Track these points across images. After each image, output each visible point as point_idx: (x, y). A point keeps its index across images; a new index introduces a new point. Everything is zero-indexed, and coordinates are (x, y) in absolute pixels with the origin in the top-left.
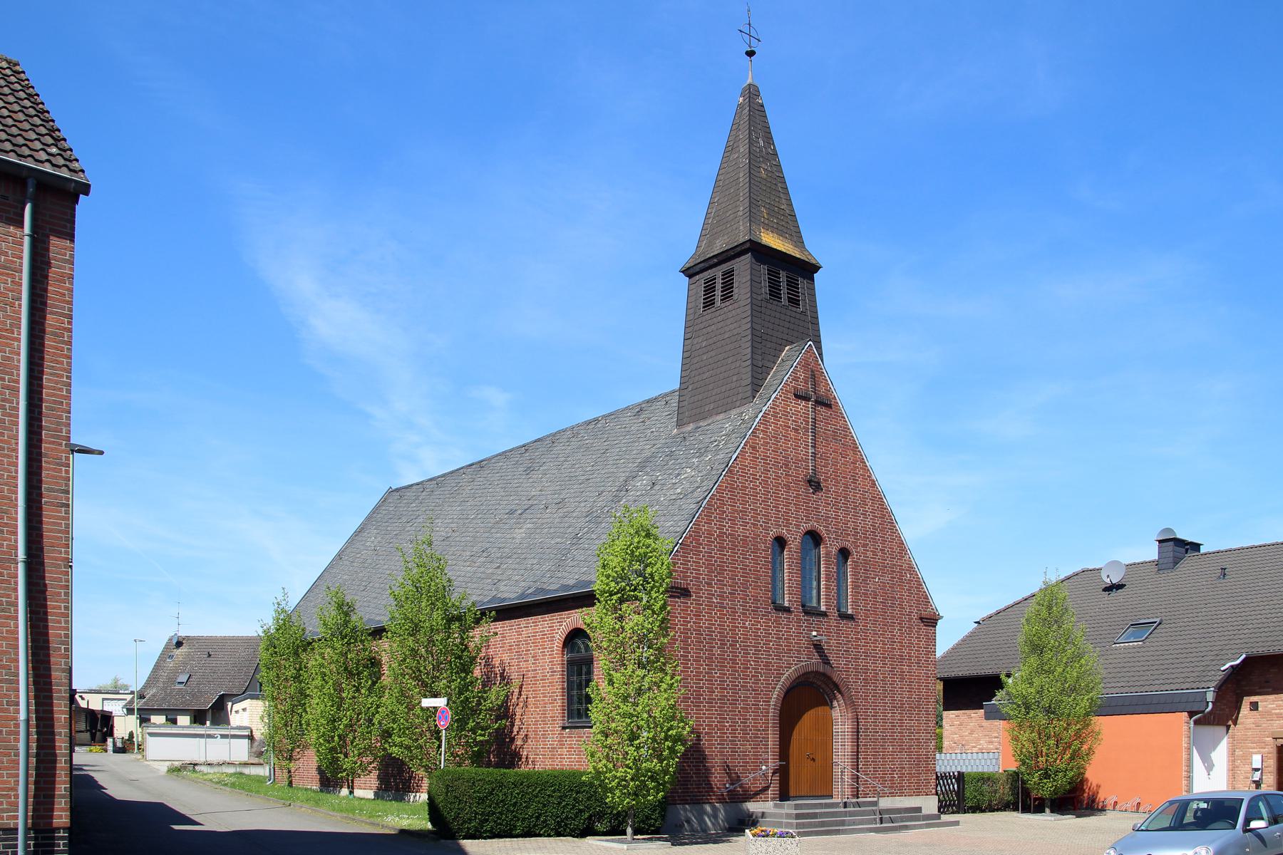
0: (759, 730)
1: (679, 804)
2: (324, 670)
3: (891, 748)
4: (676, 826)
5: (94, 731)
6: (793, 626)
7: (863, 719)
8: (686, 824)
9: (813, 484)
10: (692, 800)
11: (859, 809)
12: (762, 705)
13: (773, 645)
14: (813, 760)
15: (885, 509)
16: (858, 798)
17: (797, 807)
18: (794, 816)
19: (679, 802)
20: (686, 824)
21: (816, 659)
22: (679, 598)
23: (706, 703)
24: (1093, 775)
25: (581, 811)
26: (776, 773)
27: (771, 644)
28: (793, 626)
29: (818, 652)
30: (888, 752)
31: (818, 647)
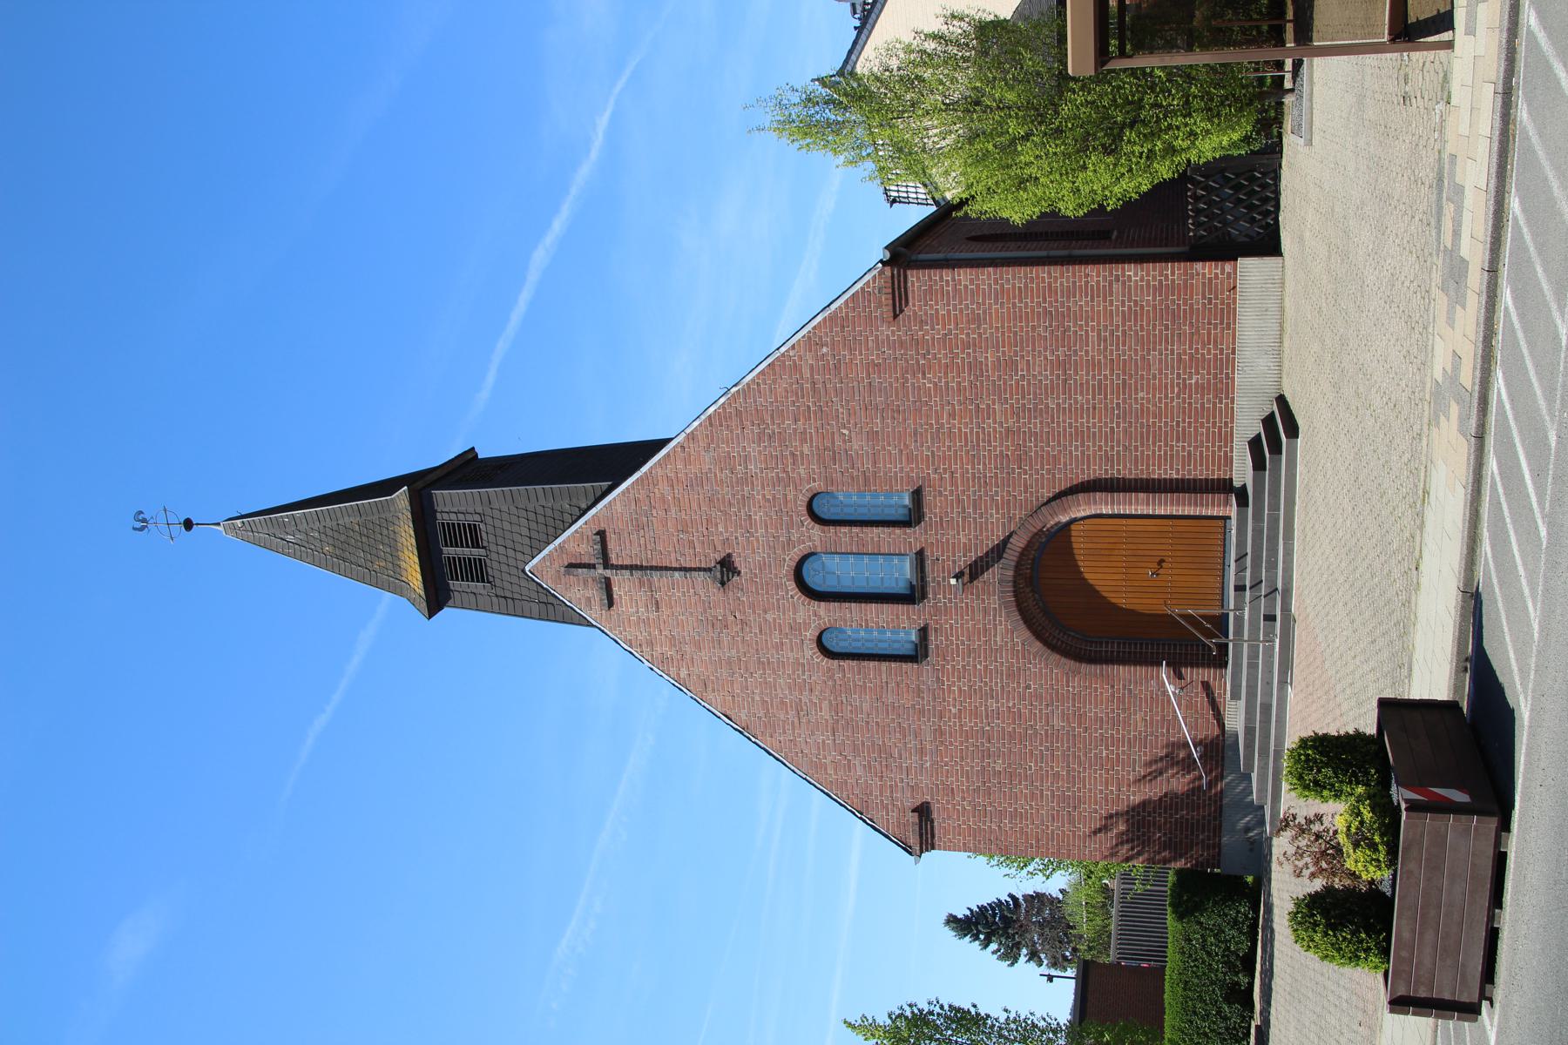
0: (1113, 696)
1: (1220, 840)
2: (1107, 882)
3: (1140, 395)
4: (1251, 850)
5: (1150, 1036)
6: (946, 621)
7: (1088, 469)
8: (1251, 834)
9: (725, 578)
10: (1215, 819)
11: (1249, 558)
12: (1074, 687)
13: (980, 663)
14: (1161, 562)
15: (724, 408)
16: (1229, 518)
17: (1236, 696)
18: (1276, 457)
19: (1217, 839)
20: (1251, 834)
21: (992, 575)
22: (932, 822)
23: (1074, 786)
24: (446, 612)
25: (1219, 1013)
26: (1180, 673)
27: (978, 667)
28: (946, 621)
29: (983, 573)
30: (1148, 399)
31: (975, 570)
